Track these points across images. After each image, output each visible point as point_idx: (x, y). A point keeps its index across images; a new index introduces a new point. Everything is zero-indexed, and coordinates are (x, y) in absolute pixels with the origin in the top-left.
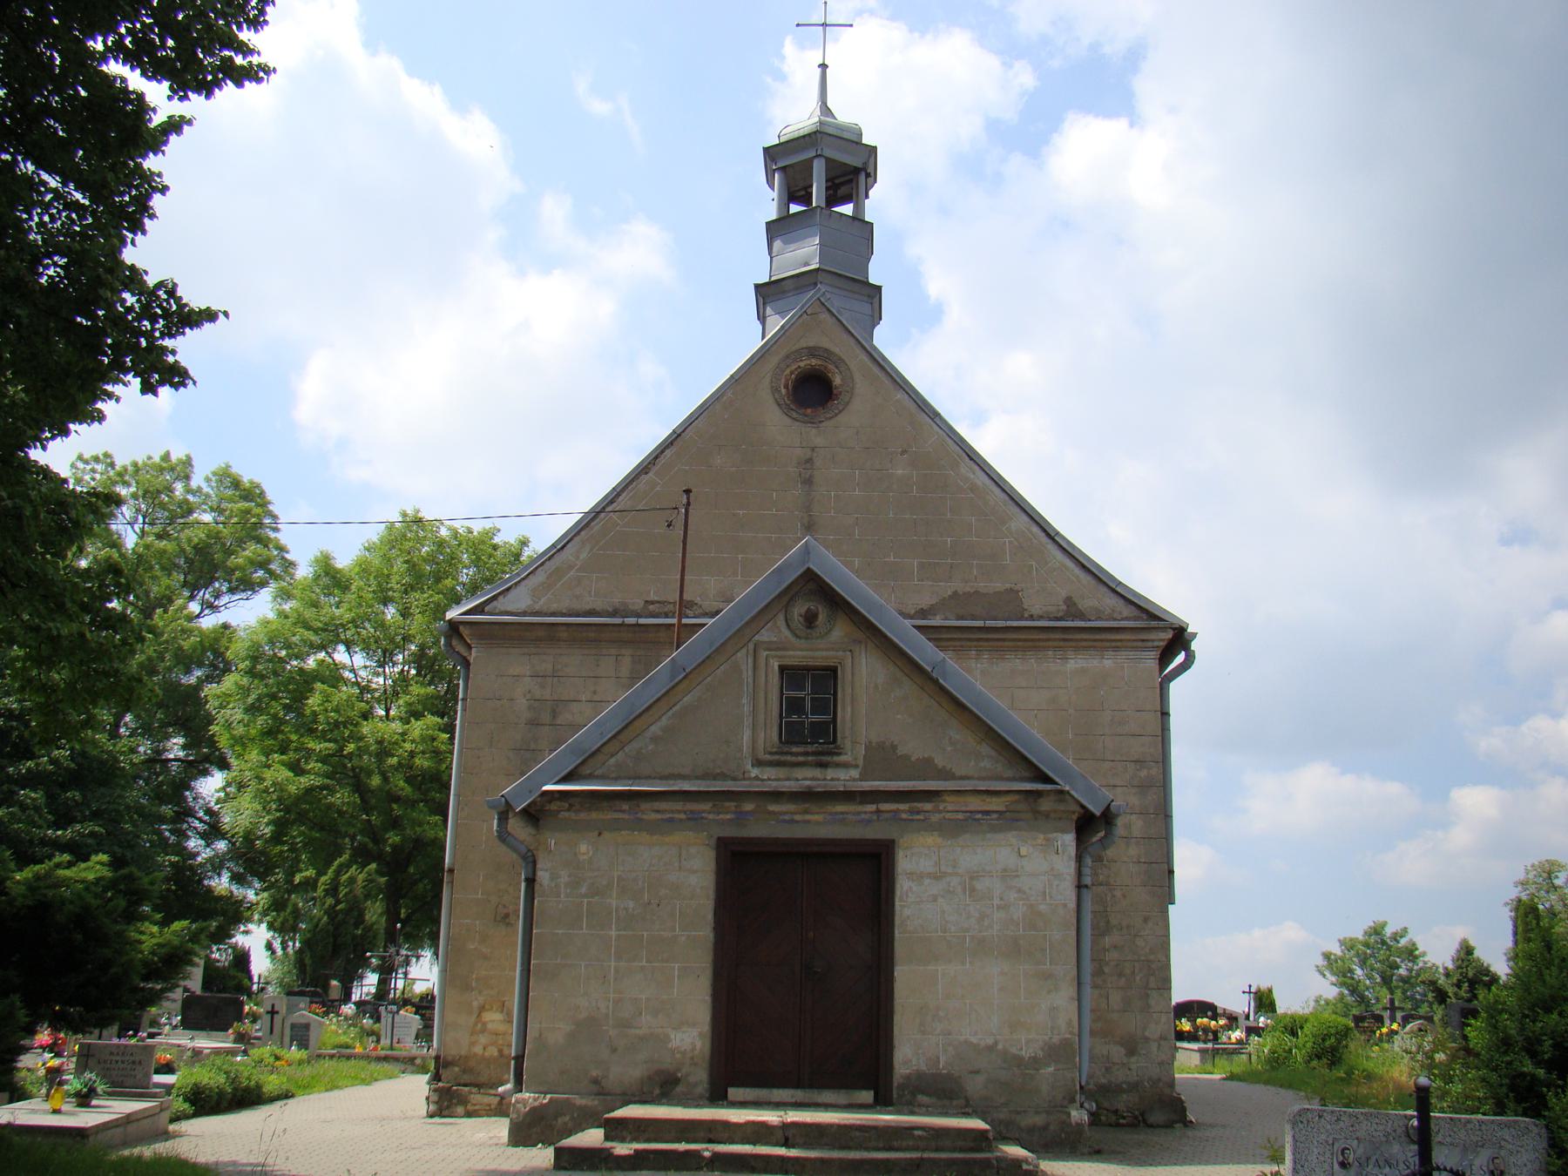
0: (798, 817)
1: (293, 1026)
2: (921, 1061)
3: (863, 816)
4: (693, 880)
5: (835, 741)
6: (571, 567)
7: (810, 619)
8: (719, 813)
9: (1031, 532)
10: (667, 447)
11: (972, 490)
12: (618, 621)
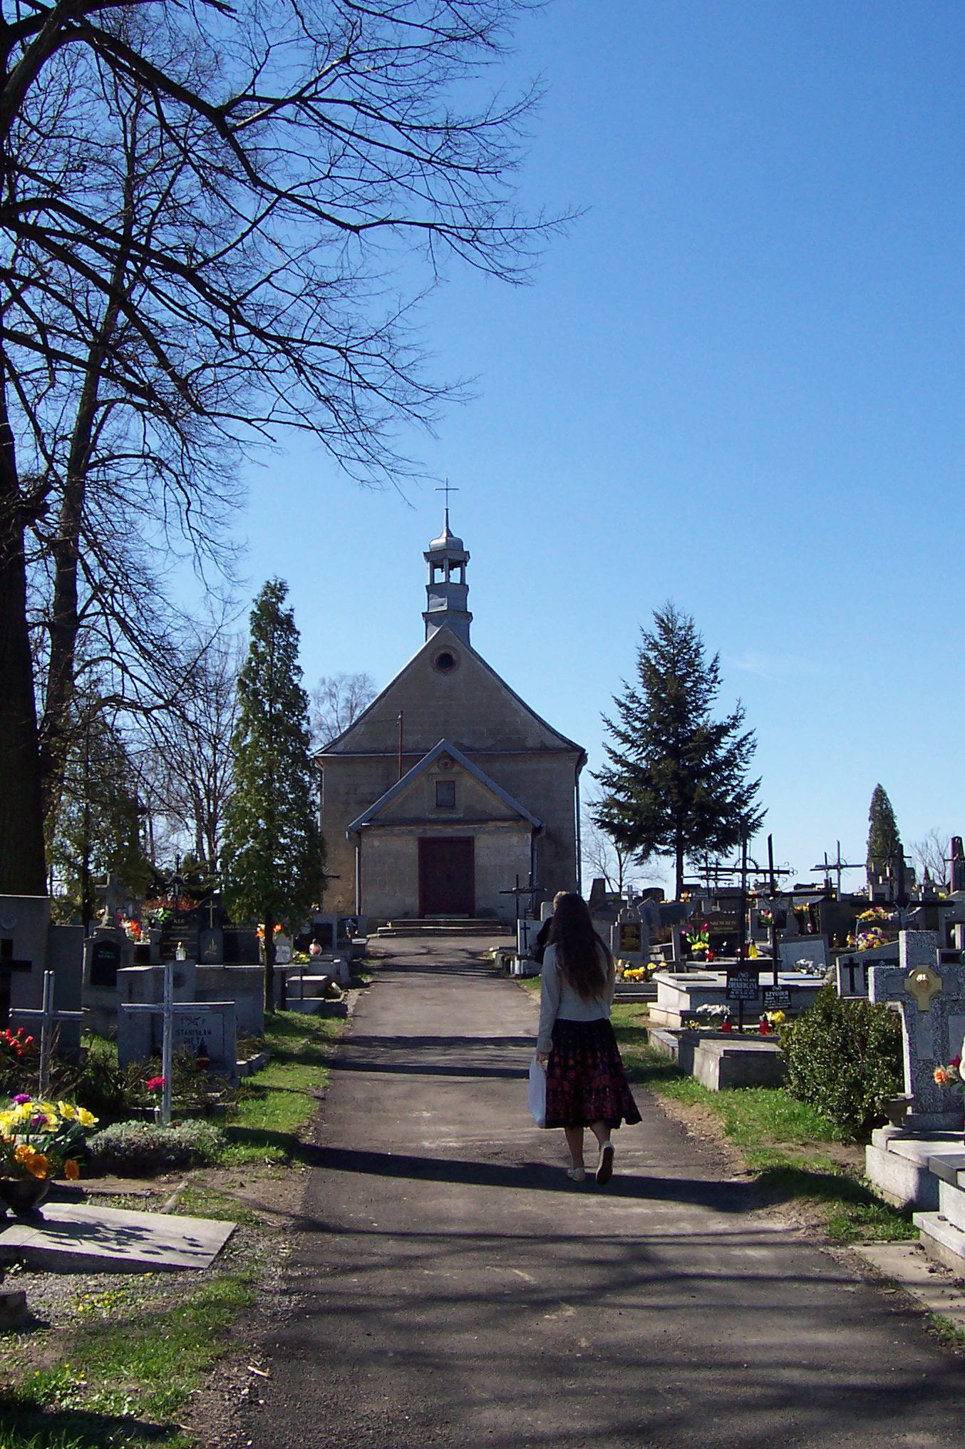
7: (446, 764)
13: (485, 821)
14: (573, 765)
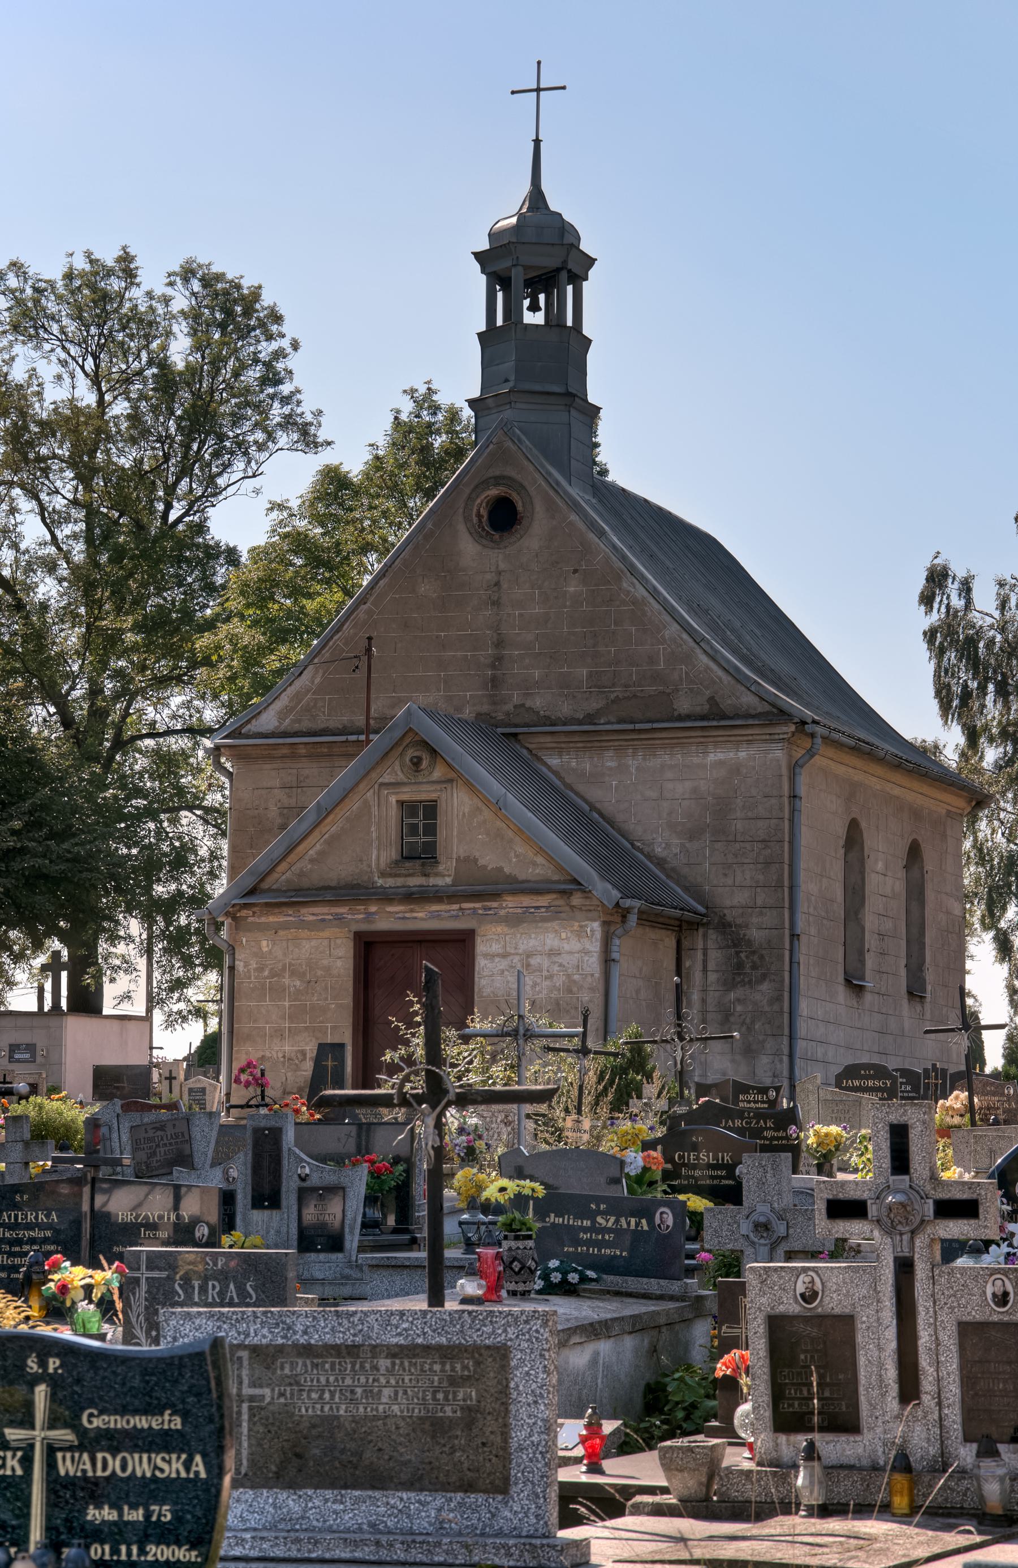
1: (191, 1090)
4: (339, 963)
6: (308, 691)
7: (416, 763)
8: (354, 914)
9: (682, 639)
10: (381, 579)
11: (633, 603)
13: (496, 896)
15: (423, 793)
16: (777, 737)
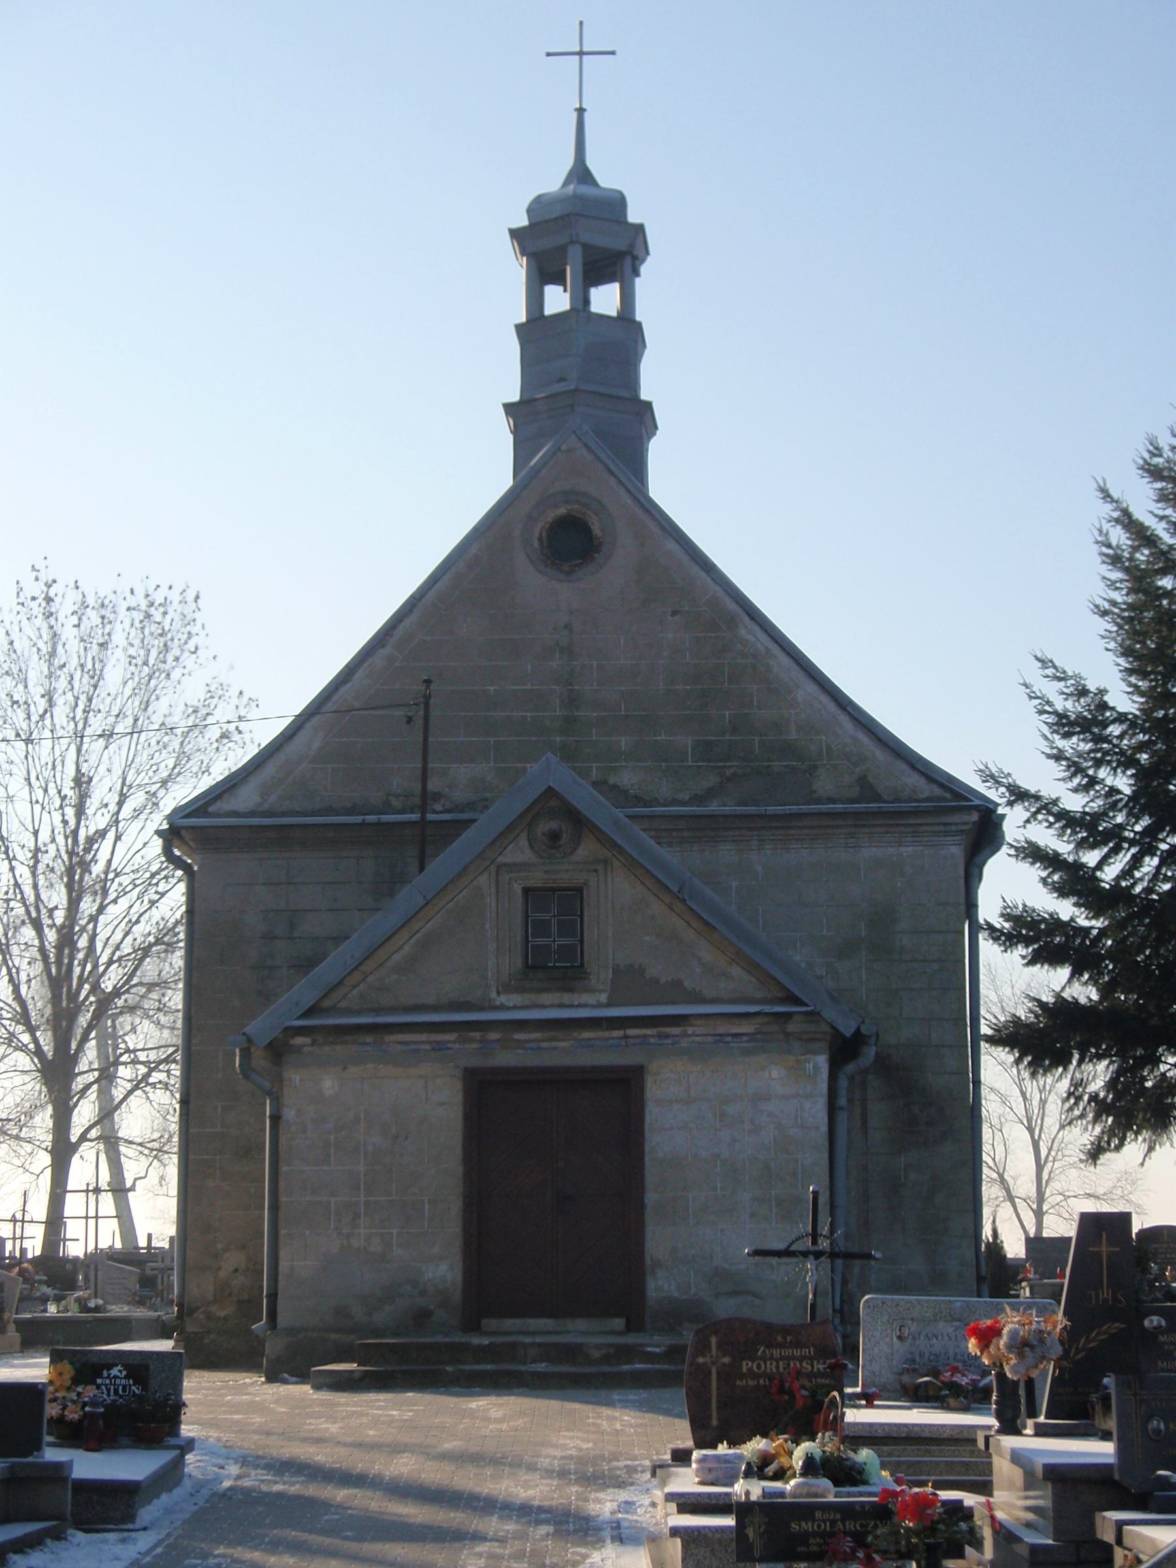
0: (545, 1045)
2: (672, 1287)
3: (611, 1042)
5: (582, 965)
12: (358, 819)
14: (955, 851)
15: (566, 873)
16: (954, 828)
